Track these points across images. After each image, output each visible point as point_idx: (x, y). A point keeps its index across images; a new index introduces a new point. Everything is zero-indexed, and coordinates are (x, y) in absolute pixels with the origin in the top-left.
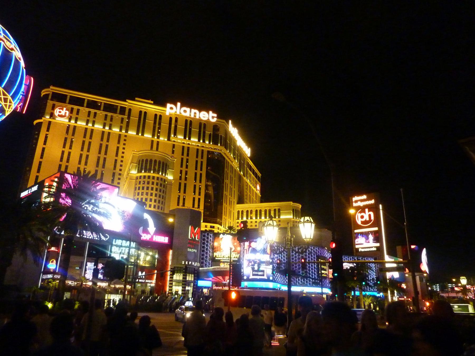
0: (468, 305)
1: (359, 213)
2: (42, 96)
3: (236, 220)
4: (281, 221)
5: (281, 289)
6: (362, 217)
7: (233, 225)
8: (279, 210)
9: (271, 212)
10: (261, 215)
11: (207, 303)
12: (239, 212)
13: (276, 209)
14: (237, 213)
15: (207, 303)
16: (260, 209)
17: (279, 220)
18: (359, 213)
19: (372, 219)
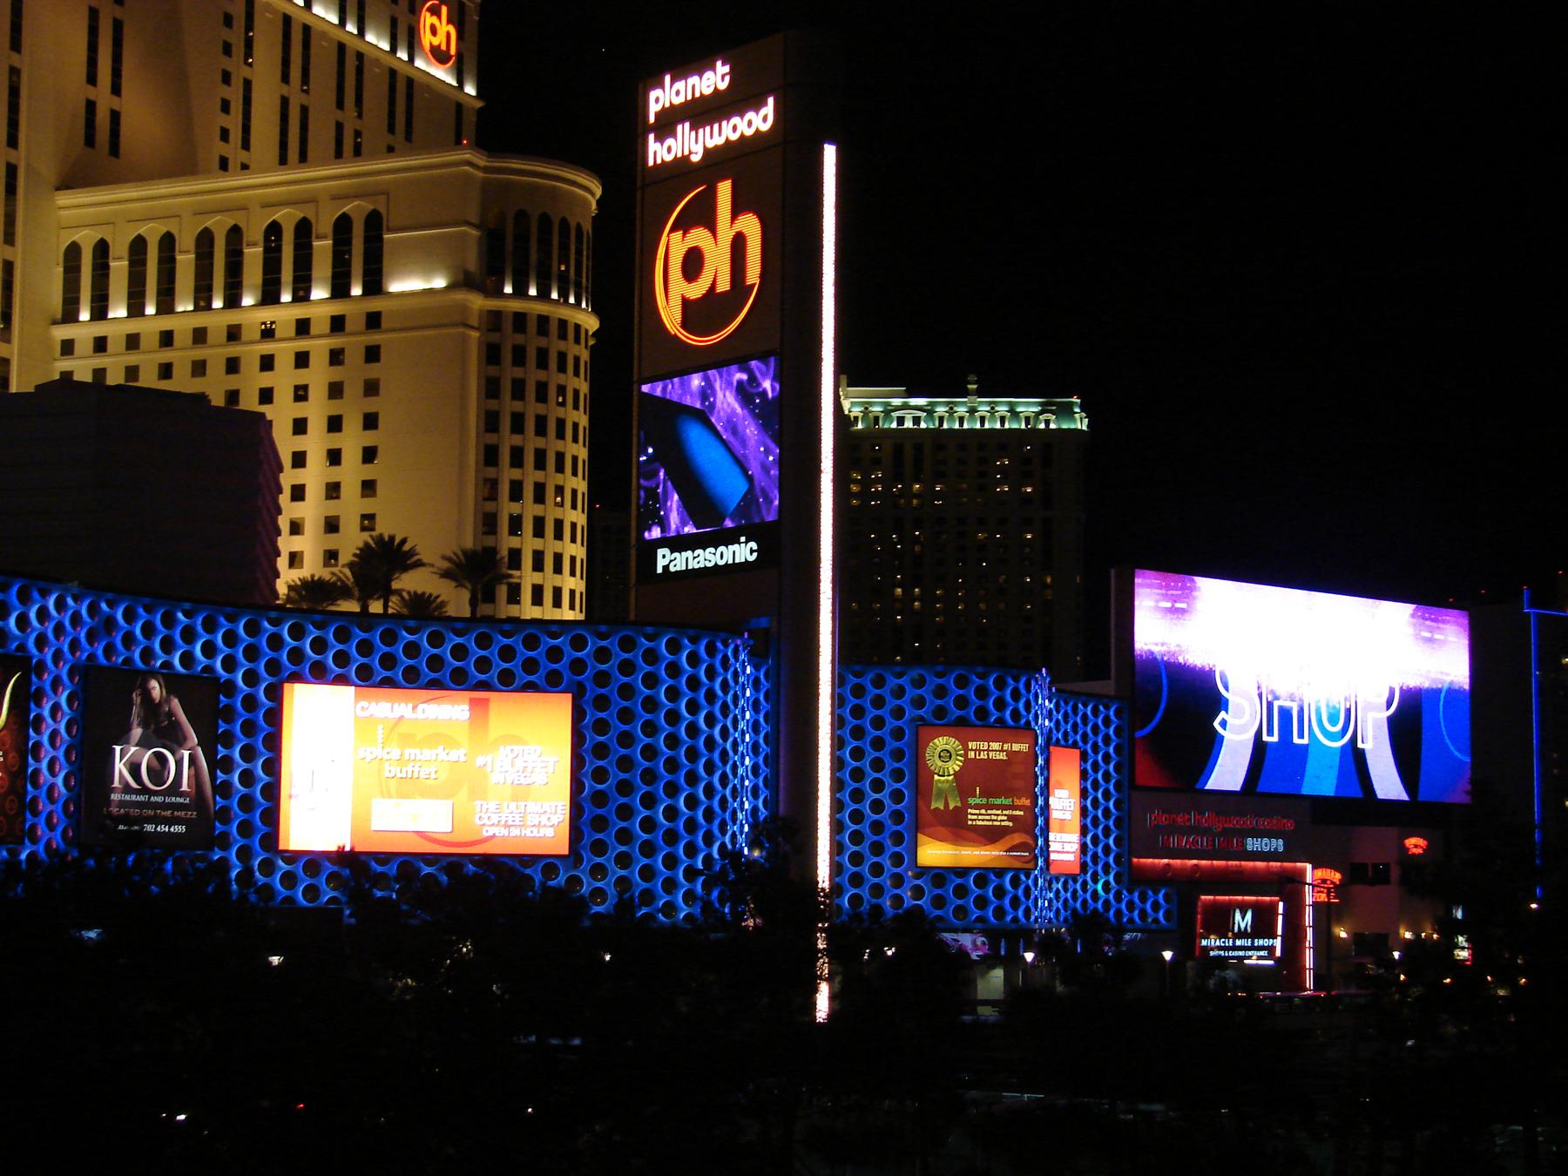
0: (1109, 679)
1: (673, 230)
2: (771, 101)
3: (55, 323)
4: (143, 339)
5: (410, 705)
6: (693, 263)
7: (213, 346)
8: (374, 224)
9: (316, 244)
10: (309, 269)
11: (650, 450)
12: (73, 252)
13: (353, 216)
14: (61, 269)
15: (650, 450)
16: (162, 229)
17: (129, 336)
18: (673, 230)
19: (749, 282)
